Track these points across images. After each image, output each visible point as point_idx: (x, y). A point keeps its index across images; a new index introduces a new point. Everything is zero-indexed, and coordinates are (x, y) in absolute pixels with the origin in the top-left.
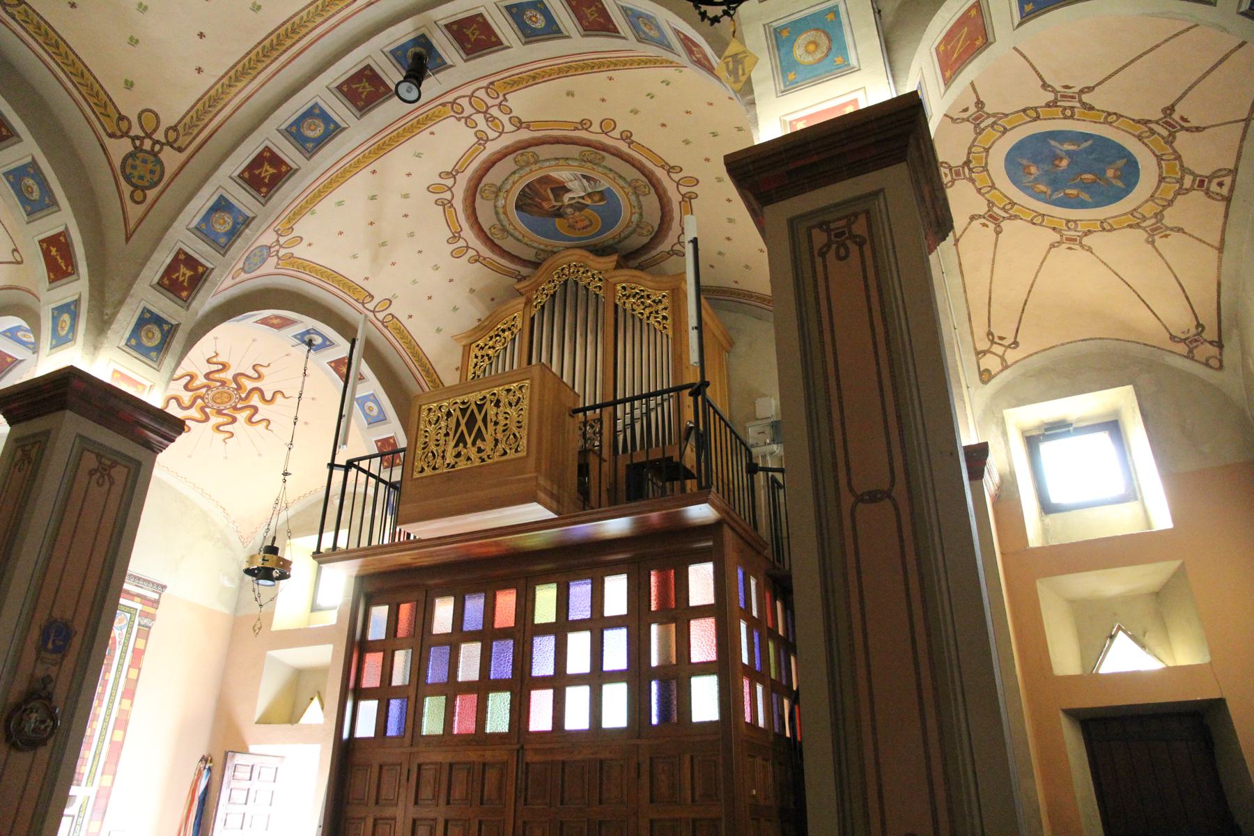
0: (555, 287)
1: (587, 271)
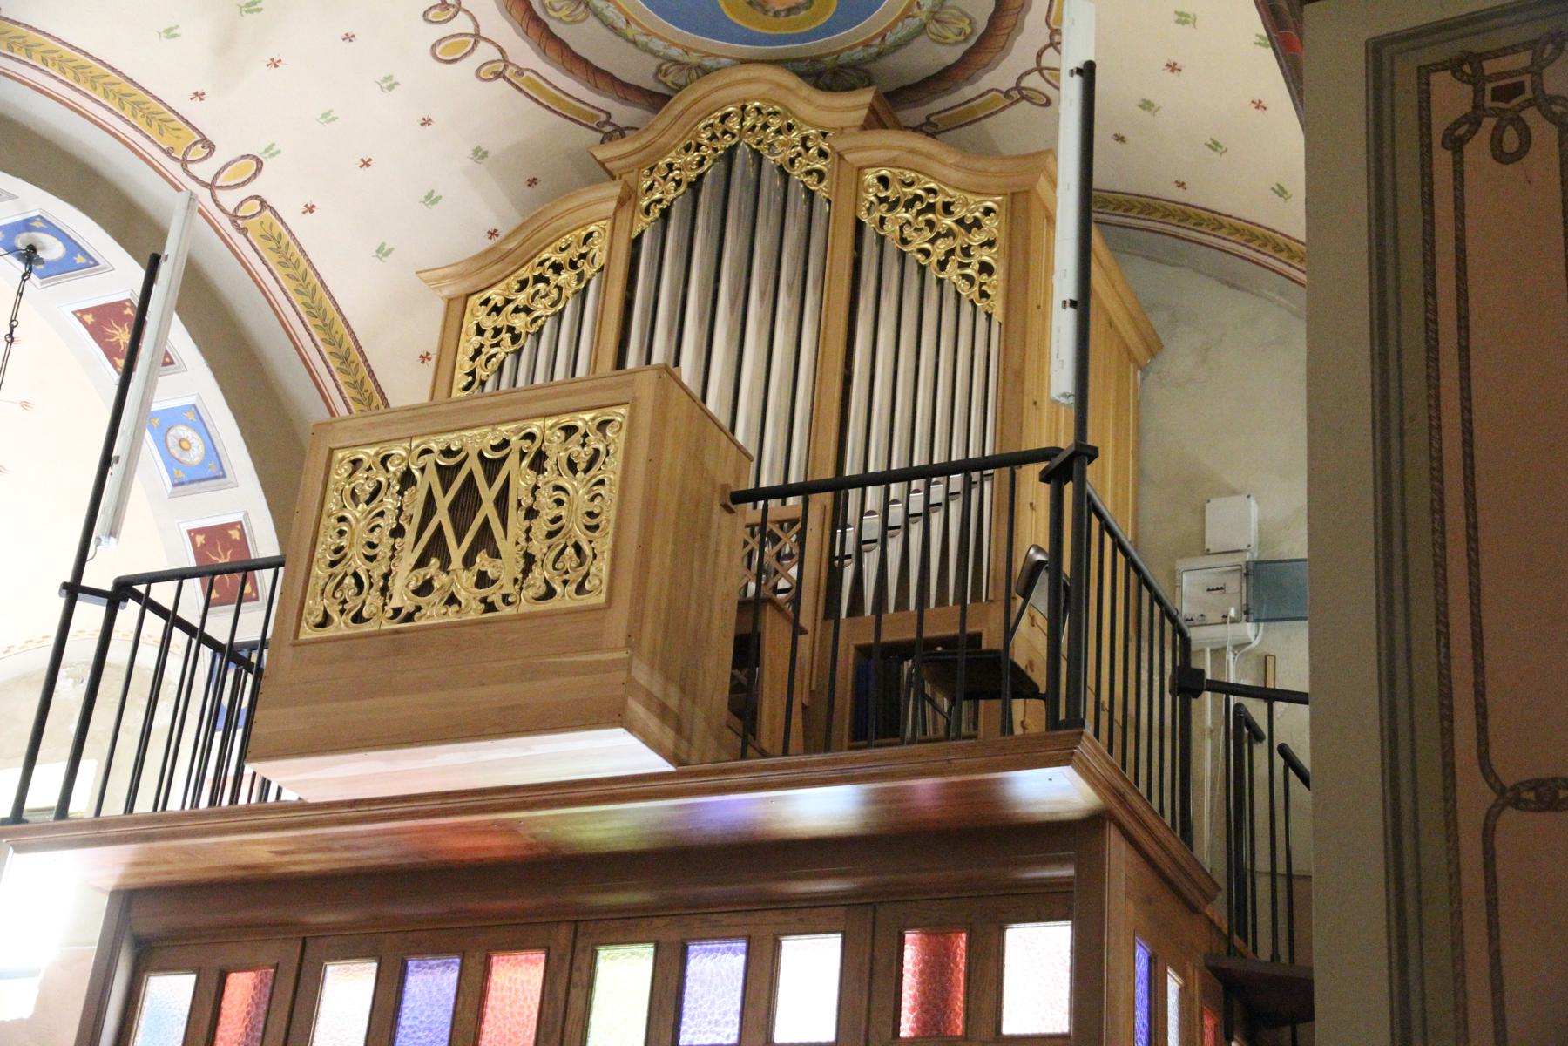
0: (700, 164)
1: (790, 127)
